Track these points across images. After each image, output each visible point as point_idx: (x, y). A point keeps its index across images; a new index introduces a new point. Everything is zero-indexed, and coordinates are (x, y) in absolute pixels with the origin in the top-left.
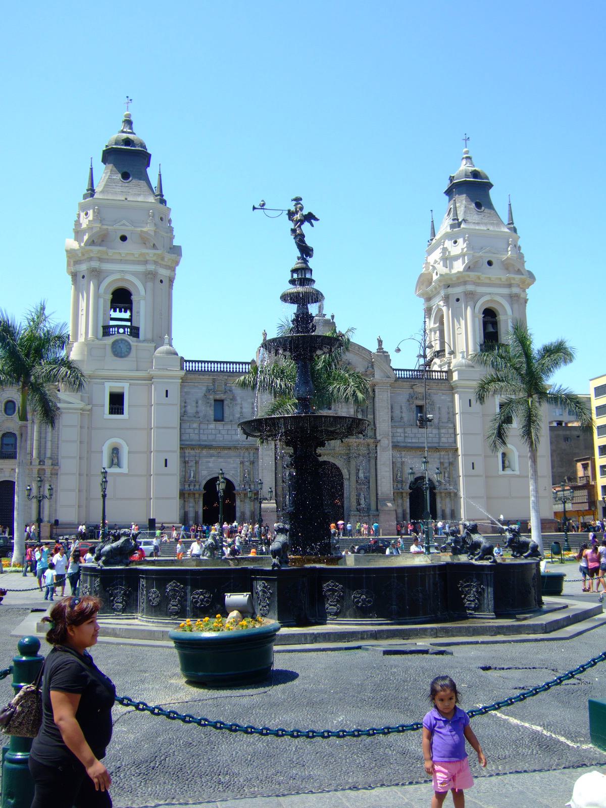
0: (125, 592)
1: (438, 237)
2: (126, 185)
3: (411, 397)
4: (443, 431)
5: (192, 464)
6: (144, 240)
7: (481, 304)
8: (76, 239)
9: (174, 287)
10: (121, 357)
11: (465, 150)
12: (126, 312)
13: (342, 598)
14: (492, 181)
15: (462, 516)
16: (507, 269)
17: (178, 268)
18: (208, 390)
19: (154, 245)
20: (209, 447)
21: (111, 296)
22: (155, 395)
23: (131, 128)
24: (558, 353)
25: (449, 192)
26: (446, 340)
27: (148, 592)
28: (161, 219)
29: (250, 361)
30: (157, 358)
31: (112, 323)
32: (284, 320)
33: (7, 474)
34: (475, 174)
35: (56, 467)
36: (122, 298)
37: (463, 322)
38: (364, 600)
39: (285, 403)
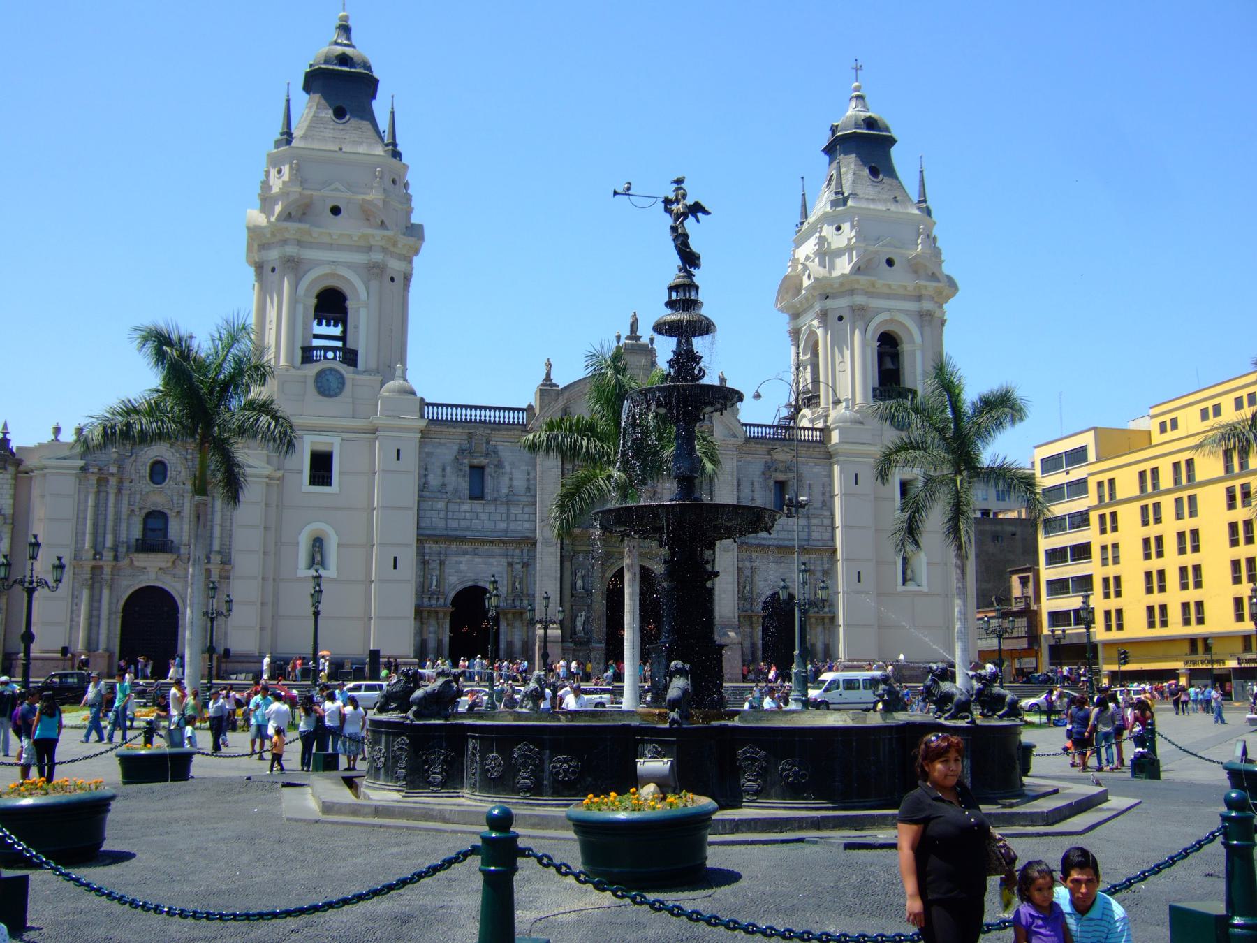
0: (446, 758)
1: (812, 219)
2: (341, 127)
3: (769, 468)
4: (814, 522)
5: (435, 565)
6: (367, 214)
7: (877, 325)
8: (263, 210)
9: (411, 289)
10: (329, 396)
11: (856, 84)
12: (336, 325)
13: (765, 770)
14: (895, 133)
15: (841, 655)
16: (916, 272)
17: (416, 260)
18: (462, 451)
19: (382, 222)
20: (462, 539)
21: (315, 301)
22: (381, 455)
23: (349, 38)
24: (1001, 407)
25: (830, 150)
26: (822, 379)
27: (483, 758)
28: (394, 182)
29: (525, 406)
30: (385, 399)
31: (316, 343)
32: (598, 347)
33: (153, 576)
34: (870, 123)
35: (227, 567)
36: (331, 304)
37: (847, 353)
38: (796, 774)
39: (595, 475)
